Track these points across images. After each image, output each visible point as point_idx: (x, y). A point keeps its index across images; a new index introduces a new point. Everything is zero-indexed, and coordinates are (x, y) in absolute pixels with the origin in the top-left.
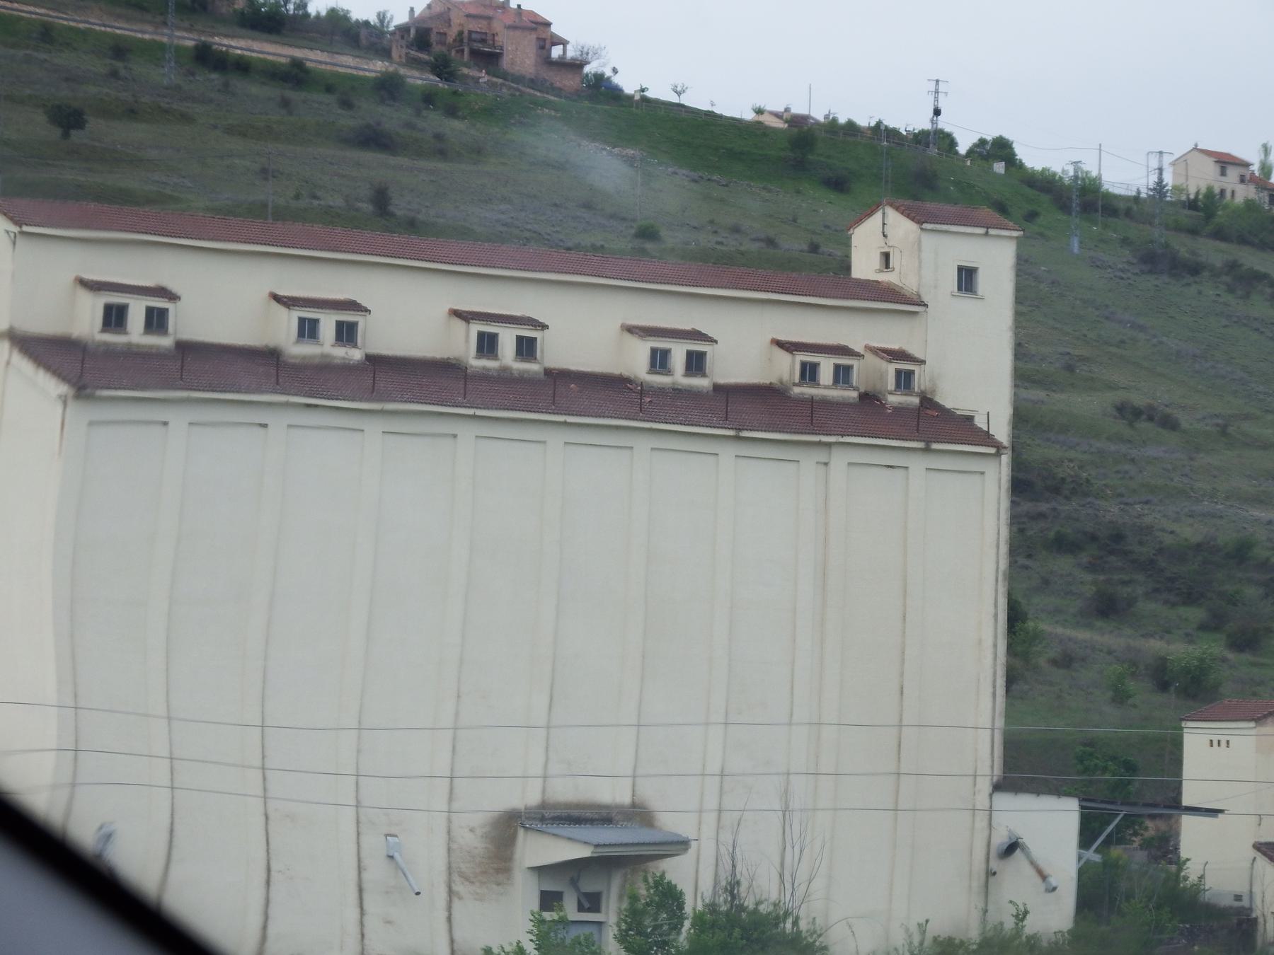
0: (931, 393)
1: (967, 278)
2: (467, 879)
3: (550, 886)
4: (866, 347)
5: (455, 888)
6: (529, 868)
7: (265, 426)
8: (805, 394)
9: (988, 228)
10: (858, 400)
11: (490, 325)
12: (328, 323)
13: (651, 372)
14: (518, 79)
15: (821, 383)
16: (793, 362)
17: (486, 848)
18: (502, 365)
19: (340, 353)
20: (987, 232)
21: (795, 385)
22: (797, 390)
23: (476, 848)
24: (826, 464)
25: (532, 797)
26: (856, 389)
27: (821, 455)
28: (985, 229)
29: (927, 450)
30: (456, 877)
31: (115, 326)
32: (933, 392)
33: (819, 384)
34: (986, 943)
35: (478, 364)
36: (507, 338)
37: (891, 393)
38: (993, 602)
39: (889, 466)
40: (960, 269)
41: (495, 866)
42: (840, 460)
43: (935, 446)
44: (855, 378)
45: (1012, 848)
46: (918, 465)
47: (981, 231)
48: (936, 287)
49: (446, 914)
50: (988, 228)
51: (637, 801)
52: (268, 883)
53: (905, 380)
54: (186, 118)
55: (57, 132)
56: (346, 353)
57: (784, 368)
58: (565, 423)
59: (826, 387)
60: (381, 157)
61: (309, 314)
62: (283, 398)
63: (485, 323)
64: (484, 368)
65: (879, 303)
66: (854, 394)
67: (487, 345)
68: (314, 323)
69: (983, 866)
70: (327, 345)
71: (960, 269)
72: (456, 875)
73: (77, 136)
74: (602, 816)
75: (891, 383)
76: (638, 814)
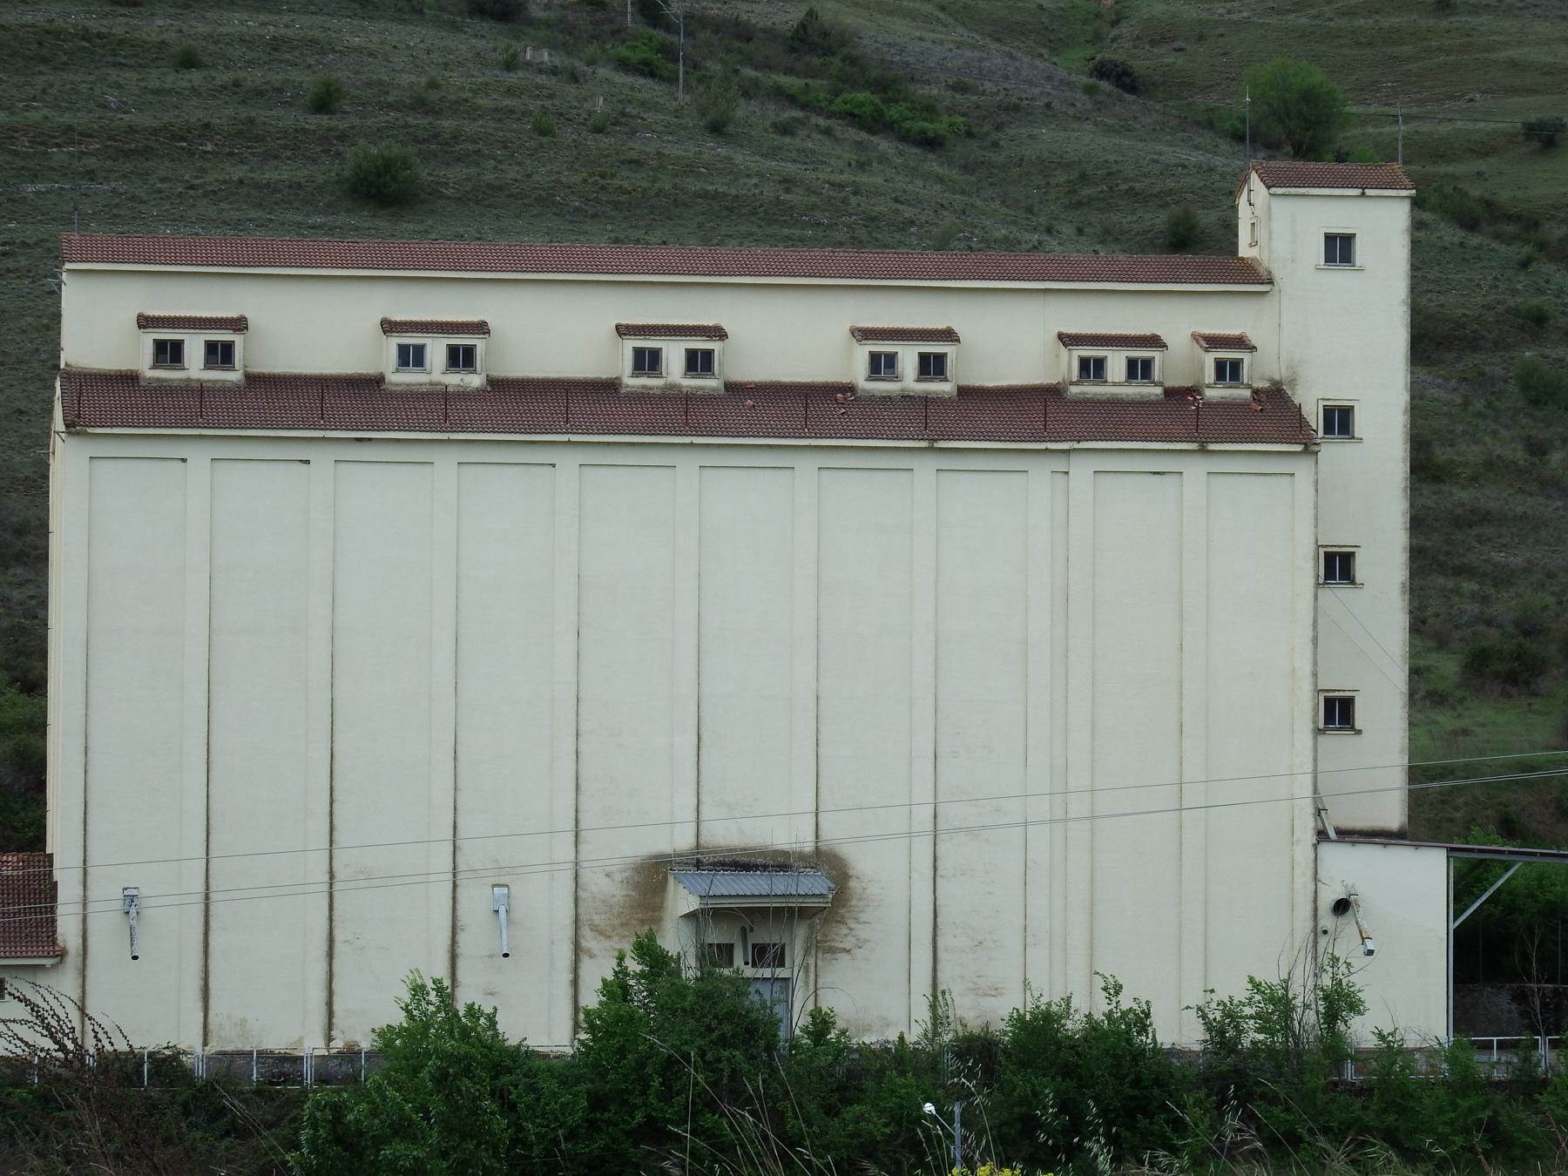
0: (1290, 382)
2: (601, 933)
3: (715, 936)
5: (584, 944)
6: (685, 916)
7: (307, 462)
8: (1087, 393)
9: (1364, 189)
10: (1162, 396)
11: (648, 339)
13: (869, 379)
15: (1109, 380)
16: (1070, 356)
17: (627, 896)
18: (668, 383)
19: (454, 380)
20: (1363, 194)
21: (1072, 383)
22: (1074, 390)
23: (613, 896)
24: (1067, 473)
26: (1160, 384)
27: (1059, 464)
28: (1361, 190)
29: (1203, 451)
30: (586, 931)
31: (463, 367)
32: (1293, 382)
33: (1106, 382)
35: (632, 382)
36: (674, 354)
37: (1208, 386)
38: (1311, 622)
39: (1155, 473)
42: (1082, 469)
43: (1212, 447)
44: (1156, 373)
45: (1342, 907)
47: (1358, 192)
48: (1293, 261)
50: (1364, 189)
51: (823, 846)
53: (1228, 372)
56: (462, 380)
59: (1115, 384)
61: (411, 339)
63: (643, 337)
64: (644, 387)
65: (1204, 285)
66: (1158, 390)
69: (1309, 924)
72: (588, 930)
74: (779, 863)
75: (1210, 375)
76: (825, 861)
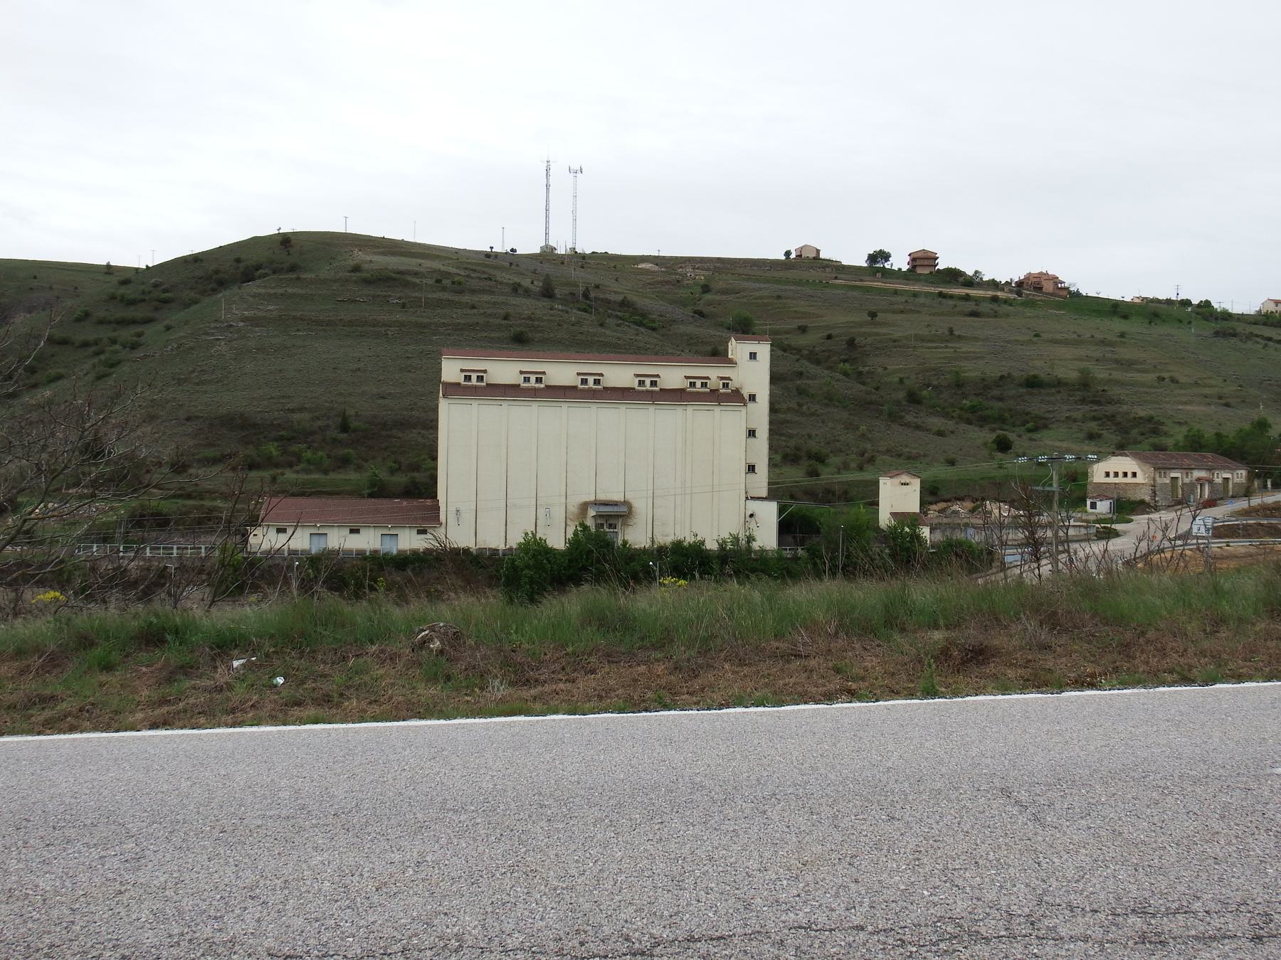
1: (753, 356)
3: (599, 522)
14: (1048, 294)
19: (537, 385)
25: (592, 499)
27: (684, 407)
29: (719, 405)
40: (751, 353)
42: (690, 409)
45: (751, 516)
46: (717, 409)
53: (726, 386)
54: (919, 312)
55: (870, 318)
57: (686, 384)
60: (976, 319)
67: (584, 382)
71: (751, 353)
73: (877, 319)
74: (615, 504)
75: (721, 387)
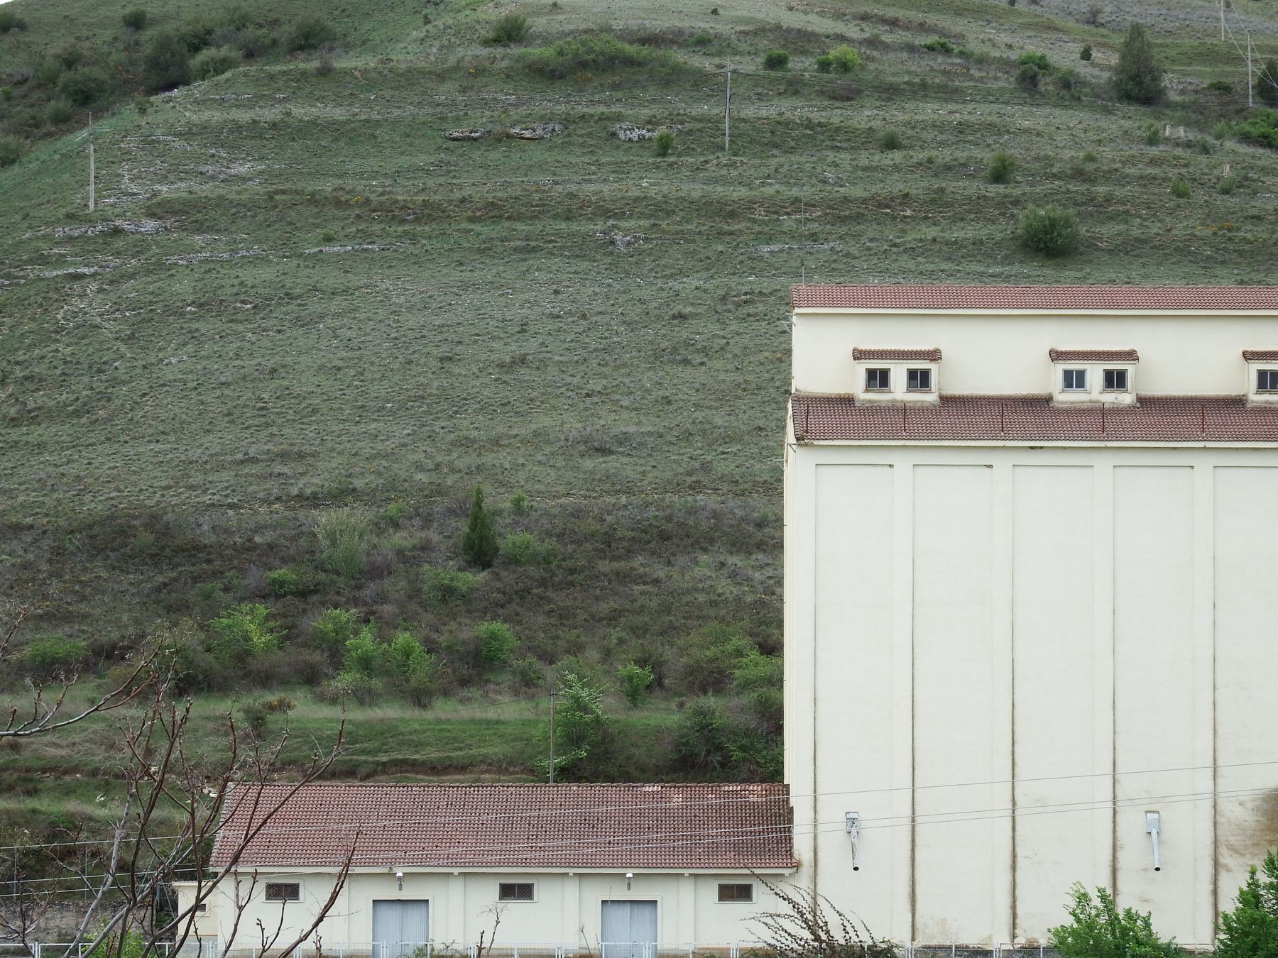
2: (1236, 851)
4: (1244, 354)
5: (1222, 860)
7: (991, 466)
12: (899, 373)
30: (1223, 850)
34: (1009, 956)
41: (1268, 838)
49: (1211, 887)
52: (1014, 868)
58: (1106, 448)
62: (1201, 444)
64: (1266, 402)
68: (1081, 375)
70: (1095, 391)
